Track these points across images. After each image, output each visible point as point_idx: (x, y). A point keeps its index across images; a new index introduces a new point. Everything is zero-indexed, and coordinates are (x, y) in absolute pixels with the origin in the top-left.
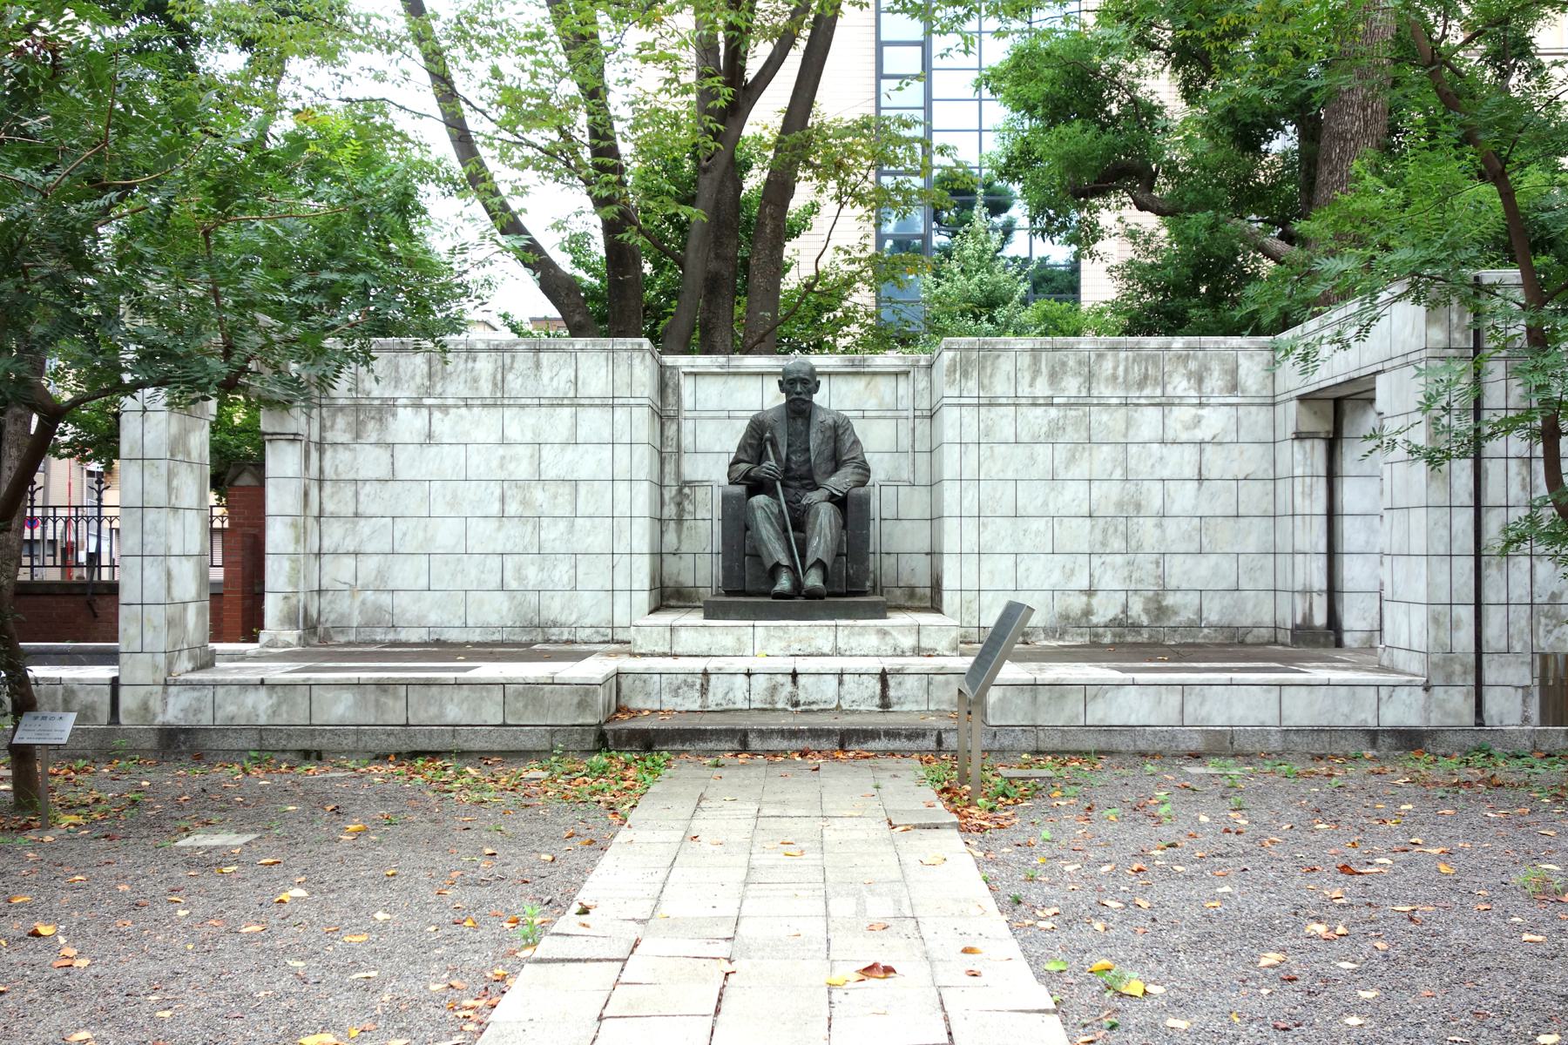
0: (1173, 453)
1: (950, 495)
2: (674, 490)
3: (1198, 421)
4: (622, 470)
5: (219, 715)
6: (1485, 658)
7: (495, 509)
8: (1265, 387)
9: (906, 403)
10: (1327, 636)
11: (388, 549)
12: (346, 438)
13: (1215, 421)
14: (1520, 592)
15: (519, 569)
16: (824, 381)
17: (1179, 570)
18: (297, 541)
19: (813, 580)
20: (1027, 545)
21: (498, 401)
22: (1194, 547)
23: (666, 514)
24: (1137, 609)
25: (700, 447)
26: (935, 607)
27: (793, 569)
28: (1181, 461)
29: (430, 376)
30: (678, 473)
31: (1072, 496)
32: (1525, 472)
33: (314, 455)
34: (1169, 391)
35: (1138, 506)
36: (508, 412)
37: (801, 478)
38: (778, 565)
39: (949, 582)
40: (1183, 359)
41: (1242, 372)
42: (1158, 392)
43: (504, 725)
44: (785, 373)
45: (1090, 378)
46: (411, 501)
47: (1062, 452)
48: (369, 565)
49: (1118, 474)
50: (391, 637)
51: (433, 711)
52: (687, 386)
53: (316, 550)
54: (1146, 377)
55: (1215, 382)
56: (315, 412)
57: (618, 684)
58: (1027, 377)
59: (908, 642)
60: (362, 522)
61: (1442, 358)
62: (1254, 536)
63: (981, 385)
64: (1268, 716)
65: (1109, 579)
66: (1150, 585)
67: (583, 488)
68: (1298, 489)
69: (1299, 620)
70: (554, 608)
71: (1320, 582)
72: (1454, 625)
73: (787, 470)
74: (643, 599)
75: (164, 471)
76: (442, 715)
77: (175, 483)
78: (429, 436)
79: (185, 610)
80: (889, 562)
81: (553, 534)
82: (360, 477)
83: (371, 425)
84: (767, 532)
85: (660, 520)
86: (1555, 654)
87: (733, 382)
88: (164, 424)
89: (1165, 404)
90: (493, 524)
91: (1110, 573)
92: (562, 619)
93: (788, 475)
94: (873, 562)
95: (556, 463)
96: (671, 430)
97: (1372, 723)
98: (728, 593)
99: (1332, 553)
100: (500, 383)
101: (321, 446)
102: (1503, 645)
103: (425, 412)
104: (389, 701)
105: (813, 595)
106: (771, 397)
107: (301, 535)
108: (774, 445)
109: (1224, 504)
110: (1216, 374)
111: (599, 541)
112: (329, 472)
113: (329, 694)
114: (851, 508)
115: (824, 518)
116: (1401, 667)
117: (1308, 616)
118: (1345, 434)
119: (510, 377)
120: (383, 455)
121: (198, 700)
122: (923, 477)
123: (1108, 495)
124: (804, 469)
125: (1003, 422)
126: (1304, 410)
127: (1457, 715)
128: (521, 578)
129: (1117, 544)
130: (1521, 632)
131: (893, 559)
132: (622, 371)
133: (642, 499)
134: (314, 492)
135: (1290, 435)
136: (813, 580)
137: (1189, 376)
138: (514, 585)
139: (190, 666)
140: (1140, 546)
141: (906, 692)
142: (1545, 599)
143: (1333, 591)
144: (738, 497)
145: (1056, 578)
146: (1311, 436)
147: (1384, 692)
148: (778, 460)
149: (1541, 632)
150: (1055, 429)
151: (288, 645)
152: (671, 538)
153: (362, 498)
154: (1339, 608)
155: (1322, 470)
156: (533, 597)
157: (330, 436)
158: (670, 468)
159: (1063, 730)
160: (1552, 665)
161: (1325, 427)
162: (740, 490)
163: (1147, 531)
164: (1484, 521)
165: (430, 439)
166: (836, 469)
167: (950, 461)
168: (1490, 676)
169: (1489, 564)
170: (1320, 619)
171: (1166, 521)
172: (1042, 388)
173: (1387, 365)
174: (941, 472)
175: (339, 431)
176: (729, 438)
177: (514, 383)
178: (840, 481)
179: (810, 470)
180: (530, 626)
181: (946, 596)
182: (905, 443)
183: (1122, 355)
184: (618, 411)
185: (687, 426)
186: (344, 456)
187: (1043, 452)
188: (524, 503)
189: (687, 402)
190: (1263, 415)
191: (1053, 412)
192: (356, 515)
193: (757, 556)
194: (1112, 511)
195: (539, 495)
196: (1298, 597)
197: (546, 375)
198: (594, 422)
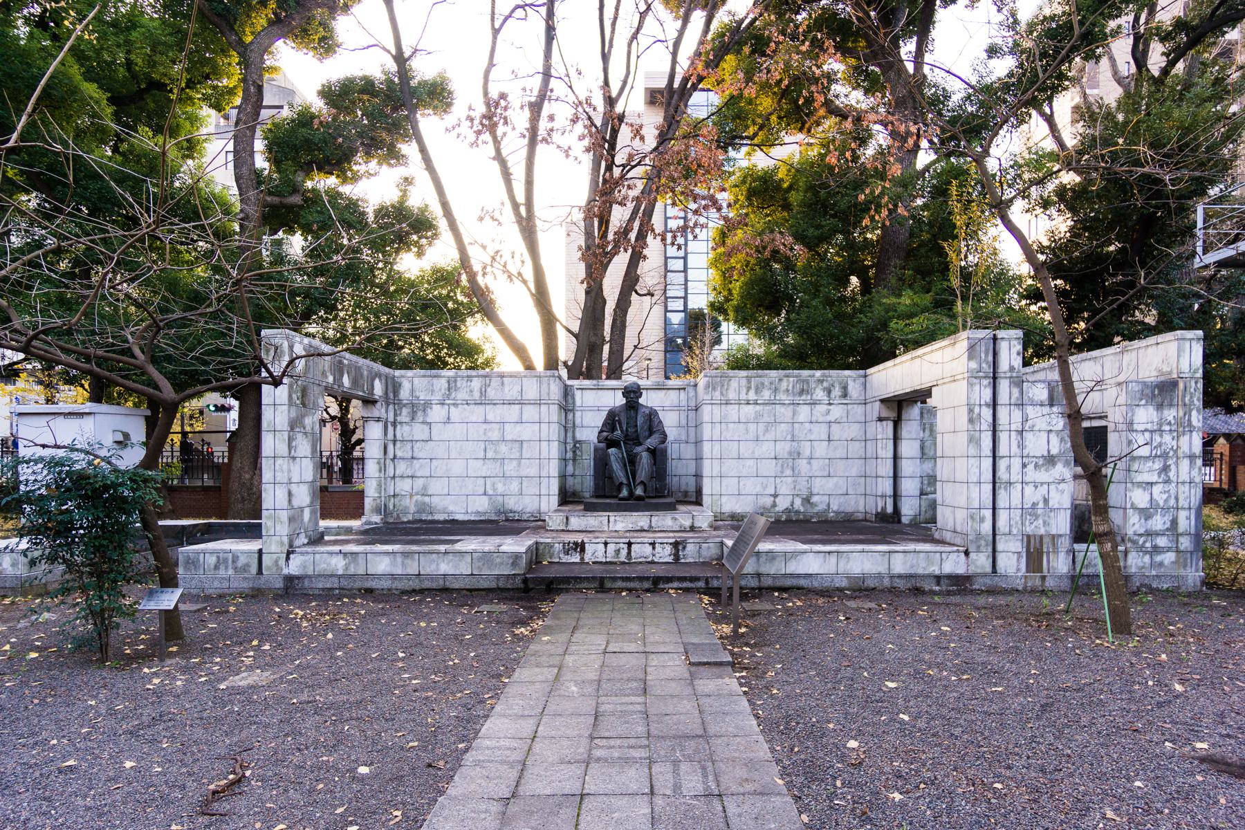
0: (815, 427)
1: (707, 448)
2: (572, 445)
3: (828, 412)
4: (544, 436)
5: (316, 569)
6: (998, 537)
7: (481, 455)
8: (861, 395)
9: (684, 403)
10: (894, 518)
11: (428, 474)
12: (407, 419)
13: (837, 412)
14: (1016, 501)
15: (493, 485)
16: (644, 392)
17: (818, 485)
18: (380, 471)
19: (639, 491)
20: (744, 473)
21: (483, 401)
22: (826, 473)
23: (568, 457)
24: (798, 503)
25: (585, 424)
26: (698, 502)
27: (629, 485)
28: (820, 432)
29: (449, 389)
30: (574, 437)
31: (766, 449)
32: (1019, 438)
33: (390, 429)
34: (814, 397)
35: (799, 454)
36: (488, 407)
37: (633, 440)
38: (621, 484)
39: (706, 490)
40: (821, 381)
41: (850, 388)
42: (809, 397)
43: (472, 575)
44: (626, 388)
45: (776, 390)
46: (440, 451)
47: (761, 427)
48: (419, 483)
49: (789, 437)
50: (430, 518)
51: (433, 566)
52: (578, 394)
53: (392, 475)
54: (803, 390)
55: (837, 392)
56: (391, 407)
57: (537, 549)
58: (745, 390)
59: (687, 523)
60: (415, 461)
61: (976, 378)
62: (855, 468)
63: (722, 394)
64: (882, 569)
65: (784, 490)
66: (805, 493)
67: (525, 445)
68: (879, 445)
69: (879, 510)
70: (512, 503)
71: (890, 491)
72: (982, 520)
73: (626, 435)
74: (555, 500)
75: (286, 437)
76: (438, 569)
77: (294, 444)
78: (449, 419)
79: (302, 511)
80: (675, 479)
81: (510, 468)
82: (415, 438)
83: (420, 413)
84: (616, 466)
85: (565, 459)
86: (1035, 536)
87: (600, 392)
88: (286, 412)
89: (814, 403)
90: (481, 462)
91: (784, 486)
92: (515, 509)
93: (627, 437)
94: (668, 480)
95: (512, 432)
96: (570, 416)
97: (937, 572)
98: (597, 497)
99: (896, 477)
100: (483, 393)
101: (394, 424)
102: (1007, 530)
103: (446, 407)
104: (408, 561)
105: (640, 498)
106: (619, 400)
107: (383, 468)
108: (620, 424)
109: (840, 453)
110: (837, 389)
111: (533, 471)
112: (399, 437)
113: (378, 558)
114: (658, 454)
115: (645, 458)
116: (948, 540)
117: (884, 509)
118: (903, 417)
119: (489, 390)
120: (426, 428)
121: (305, 561)
122: (692, 439)
123: (784, 448)
124: (634, 435)
125: (732, 411)
126: (883, 406)
127: (983, 567)
128: (495, 490)
129: (788, 472)
130: (1017, 523)
131: (677, 478)
132: (544, 386)
133: (554, 450)
134: (390, 447)
135: (875, 418)
136: (639, 491)
137: (824, 389)
138: (491, 492)
139: (306, 541)
140: (799, 473)
141: (690, 553)
142: (1029, 506)
143: (896, 496)
144: (602, 449)
145: (758, 489)
146: (886, 419)
147: (944, 555)
148: (622, 431)
149: (1027, 523)
150: (758, 415)
151: (376, 523)
152: (570, 469)
153: (415, 449)
154: (899, 504)
155: (891, 436)
156: (500, 499)
157: (399, 419)
158: (570, 434)
159: (774, 577)
160: (1032, 541)
161: (893, 415)
162: (602, 445)
163: (803, 465)
164: (997, 464)
165: (448, 420)
166: (650, 435)
167: (707, 432)
168: (1000, 547)
169: (1000, 488)
170: (890, 509)
171: (812, 461)
172: (752, 396)
173: (941, 382)
174: (702, 436)
175: (404, 415)
176: (599, 420)
177: (491, 393)
178: (651, 442)
179: (638, 436)
180: (499, 513)
181: (705, 498)
182: (684, 422)
183: (791, 379)
184: (542, 406)
185: (578, 414)
186: (406, 428)
187: (752, 427)
188: (495, 452)
189: (578, 402)
190: (860, 409)
191: (758, 407)
192: (413, 458)
193: (611, 478)
194: (786, 456)
195: (503, 448)
196: (879, 498)
197: (507, 389)
198: (530, 412)
